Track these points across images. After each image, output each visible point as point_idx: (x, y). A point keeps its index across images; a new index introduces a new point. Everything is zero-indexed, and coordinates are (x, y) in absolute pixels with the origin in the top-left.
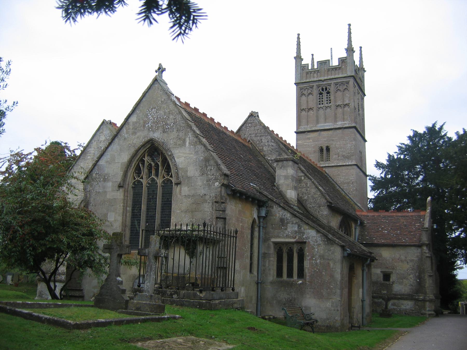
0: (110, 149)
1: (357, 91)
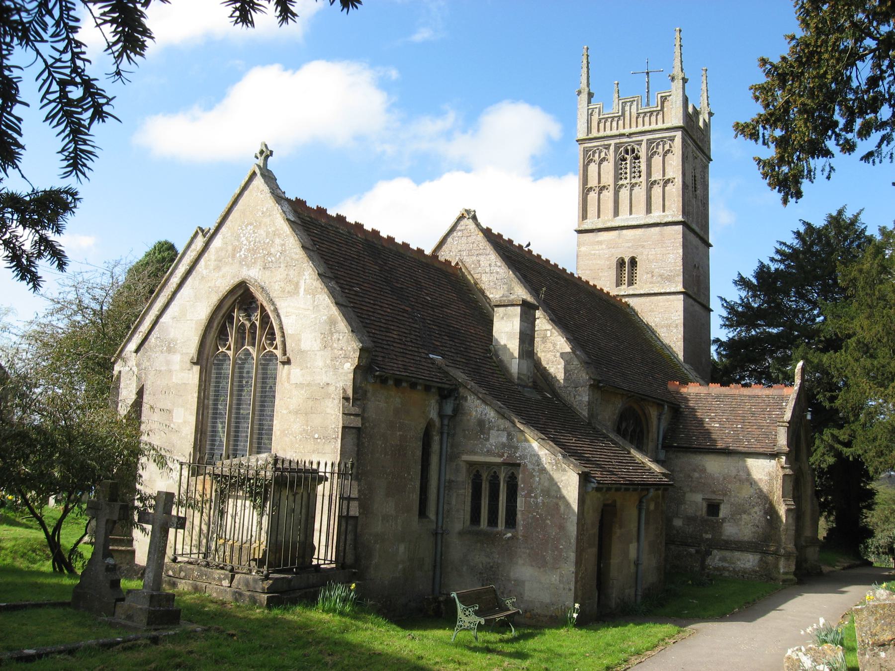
0: (179, 295)
1: (690, 154)
